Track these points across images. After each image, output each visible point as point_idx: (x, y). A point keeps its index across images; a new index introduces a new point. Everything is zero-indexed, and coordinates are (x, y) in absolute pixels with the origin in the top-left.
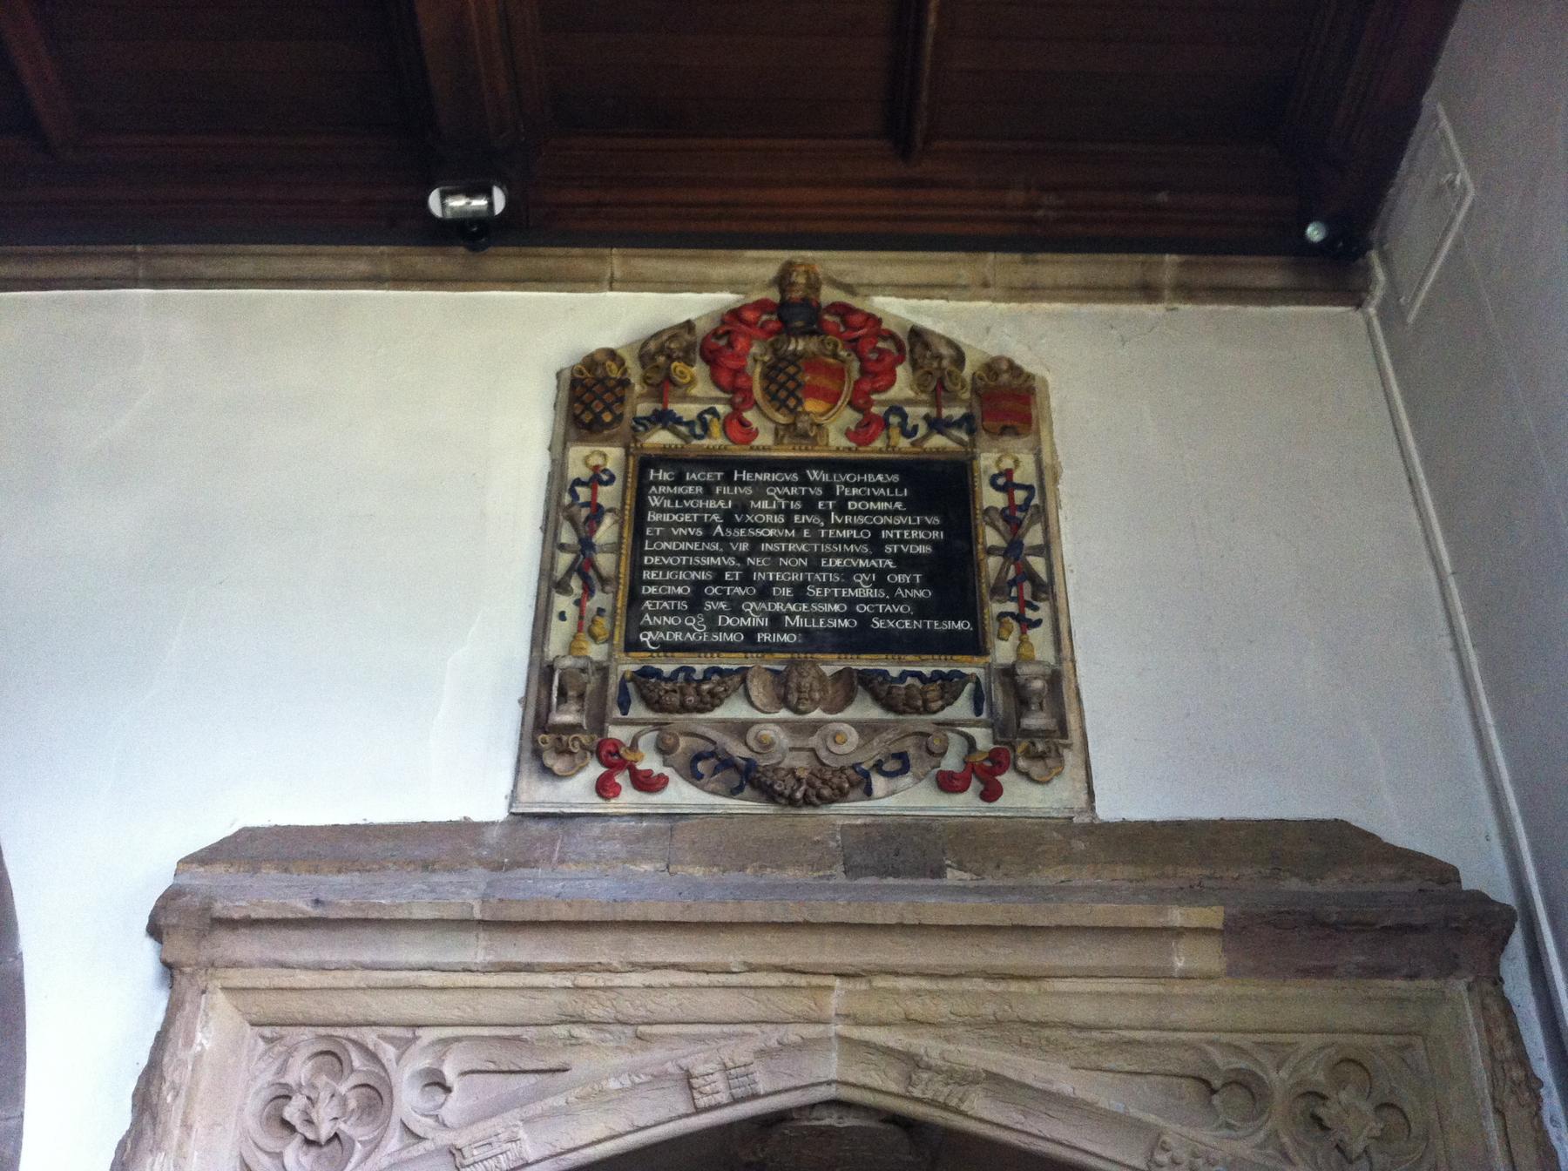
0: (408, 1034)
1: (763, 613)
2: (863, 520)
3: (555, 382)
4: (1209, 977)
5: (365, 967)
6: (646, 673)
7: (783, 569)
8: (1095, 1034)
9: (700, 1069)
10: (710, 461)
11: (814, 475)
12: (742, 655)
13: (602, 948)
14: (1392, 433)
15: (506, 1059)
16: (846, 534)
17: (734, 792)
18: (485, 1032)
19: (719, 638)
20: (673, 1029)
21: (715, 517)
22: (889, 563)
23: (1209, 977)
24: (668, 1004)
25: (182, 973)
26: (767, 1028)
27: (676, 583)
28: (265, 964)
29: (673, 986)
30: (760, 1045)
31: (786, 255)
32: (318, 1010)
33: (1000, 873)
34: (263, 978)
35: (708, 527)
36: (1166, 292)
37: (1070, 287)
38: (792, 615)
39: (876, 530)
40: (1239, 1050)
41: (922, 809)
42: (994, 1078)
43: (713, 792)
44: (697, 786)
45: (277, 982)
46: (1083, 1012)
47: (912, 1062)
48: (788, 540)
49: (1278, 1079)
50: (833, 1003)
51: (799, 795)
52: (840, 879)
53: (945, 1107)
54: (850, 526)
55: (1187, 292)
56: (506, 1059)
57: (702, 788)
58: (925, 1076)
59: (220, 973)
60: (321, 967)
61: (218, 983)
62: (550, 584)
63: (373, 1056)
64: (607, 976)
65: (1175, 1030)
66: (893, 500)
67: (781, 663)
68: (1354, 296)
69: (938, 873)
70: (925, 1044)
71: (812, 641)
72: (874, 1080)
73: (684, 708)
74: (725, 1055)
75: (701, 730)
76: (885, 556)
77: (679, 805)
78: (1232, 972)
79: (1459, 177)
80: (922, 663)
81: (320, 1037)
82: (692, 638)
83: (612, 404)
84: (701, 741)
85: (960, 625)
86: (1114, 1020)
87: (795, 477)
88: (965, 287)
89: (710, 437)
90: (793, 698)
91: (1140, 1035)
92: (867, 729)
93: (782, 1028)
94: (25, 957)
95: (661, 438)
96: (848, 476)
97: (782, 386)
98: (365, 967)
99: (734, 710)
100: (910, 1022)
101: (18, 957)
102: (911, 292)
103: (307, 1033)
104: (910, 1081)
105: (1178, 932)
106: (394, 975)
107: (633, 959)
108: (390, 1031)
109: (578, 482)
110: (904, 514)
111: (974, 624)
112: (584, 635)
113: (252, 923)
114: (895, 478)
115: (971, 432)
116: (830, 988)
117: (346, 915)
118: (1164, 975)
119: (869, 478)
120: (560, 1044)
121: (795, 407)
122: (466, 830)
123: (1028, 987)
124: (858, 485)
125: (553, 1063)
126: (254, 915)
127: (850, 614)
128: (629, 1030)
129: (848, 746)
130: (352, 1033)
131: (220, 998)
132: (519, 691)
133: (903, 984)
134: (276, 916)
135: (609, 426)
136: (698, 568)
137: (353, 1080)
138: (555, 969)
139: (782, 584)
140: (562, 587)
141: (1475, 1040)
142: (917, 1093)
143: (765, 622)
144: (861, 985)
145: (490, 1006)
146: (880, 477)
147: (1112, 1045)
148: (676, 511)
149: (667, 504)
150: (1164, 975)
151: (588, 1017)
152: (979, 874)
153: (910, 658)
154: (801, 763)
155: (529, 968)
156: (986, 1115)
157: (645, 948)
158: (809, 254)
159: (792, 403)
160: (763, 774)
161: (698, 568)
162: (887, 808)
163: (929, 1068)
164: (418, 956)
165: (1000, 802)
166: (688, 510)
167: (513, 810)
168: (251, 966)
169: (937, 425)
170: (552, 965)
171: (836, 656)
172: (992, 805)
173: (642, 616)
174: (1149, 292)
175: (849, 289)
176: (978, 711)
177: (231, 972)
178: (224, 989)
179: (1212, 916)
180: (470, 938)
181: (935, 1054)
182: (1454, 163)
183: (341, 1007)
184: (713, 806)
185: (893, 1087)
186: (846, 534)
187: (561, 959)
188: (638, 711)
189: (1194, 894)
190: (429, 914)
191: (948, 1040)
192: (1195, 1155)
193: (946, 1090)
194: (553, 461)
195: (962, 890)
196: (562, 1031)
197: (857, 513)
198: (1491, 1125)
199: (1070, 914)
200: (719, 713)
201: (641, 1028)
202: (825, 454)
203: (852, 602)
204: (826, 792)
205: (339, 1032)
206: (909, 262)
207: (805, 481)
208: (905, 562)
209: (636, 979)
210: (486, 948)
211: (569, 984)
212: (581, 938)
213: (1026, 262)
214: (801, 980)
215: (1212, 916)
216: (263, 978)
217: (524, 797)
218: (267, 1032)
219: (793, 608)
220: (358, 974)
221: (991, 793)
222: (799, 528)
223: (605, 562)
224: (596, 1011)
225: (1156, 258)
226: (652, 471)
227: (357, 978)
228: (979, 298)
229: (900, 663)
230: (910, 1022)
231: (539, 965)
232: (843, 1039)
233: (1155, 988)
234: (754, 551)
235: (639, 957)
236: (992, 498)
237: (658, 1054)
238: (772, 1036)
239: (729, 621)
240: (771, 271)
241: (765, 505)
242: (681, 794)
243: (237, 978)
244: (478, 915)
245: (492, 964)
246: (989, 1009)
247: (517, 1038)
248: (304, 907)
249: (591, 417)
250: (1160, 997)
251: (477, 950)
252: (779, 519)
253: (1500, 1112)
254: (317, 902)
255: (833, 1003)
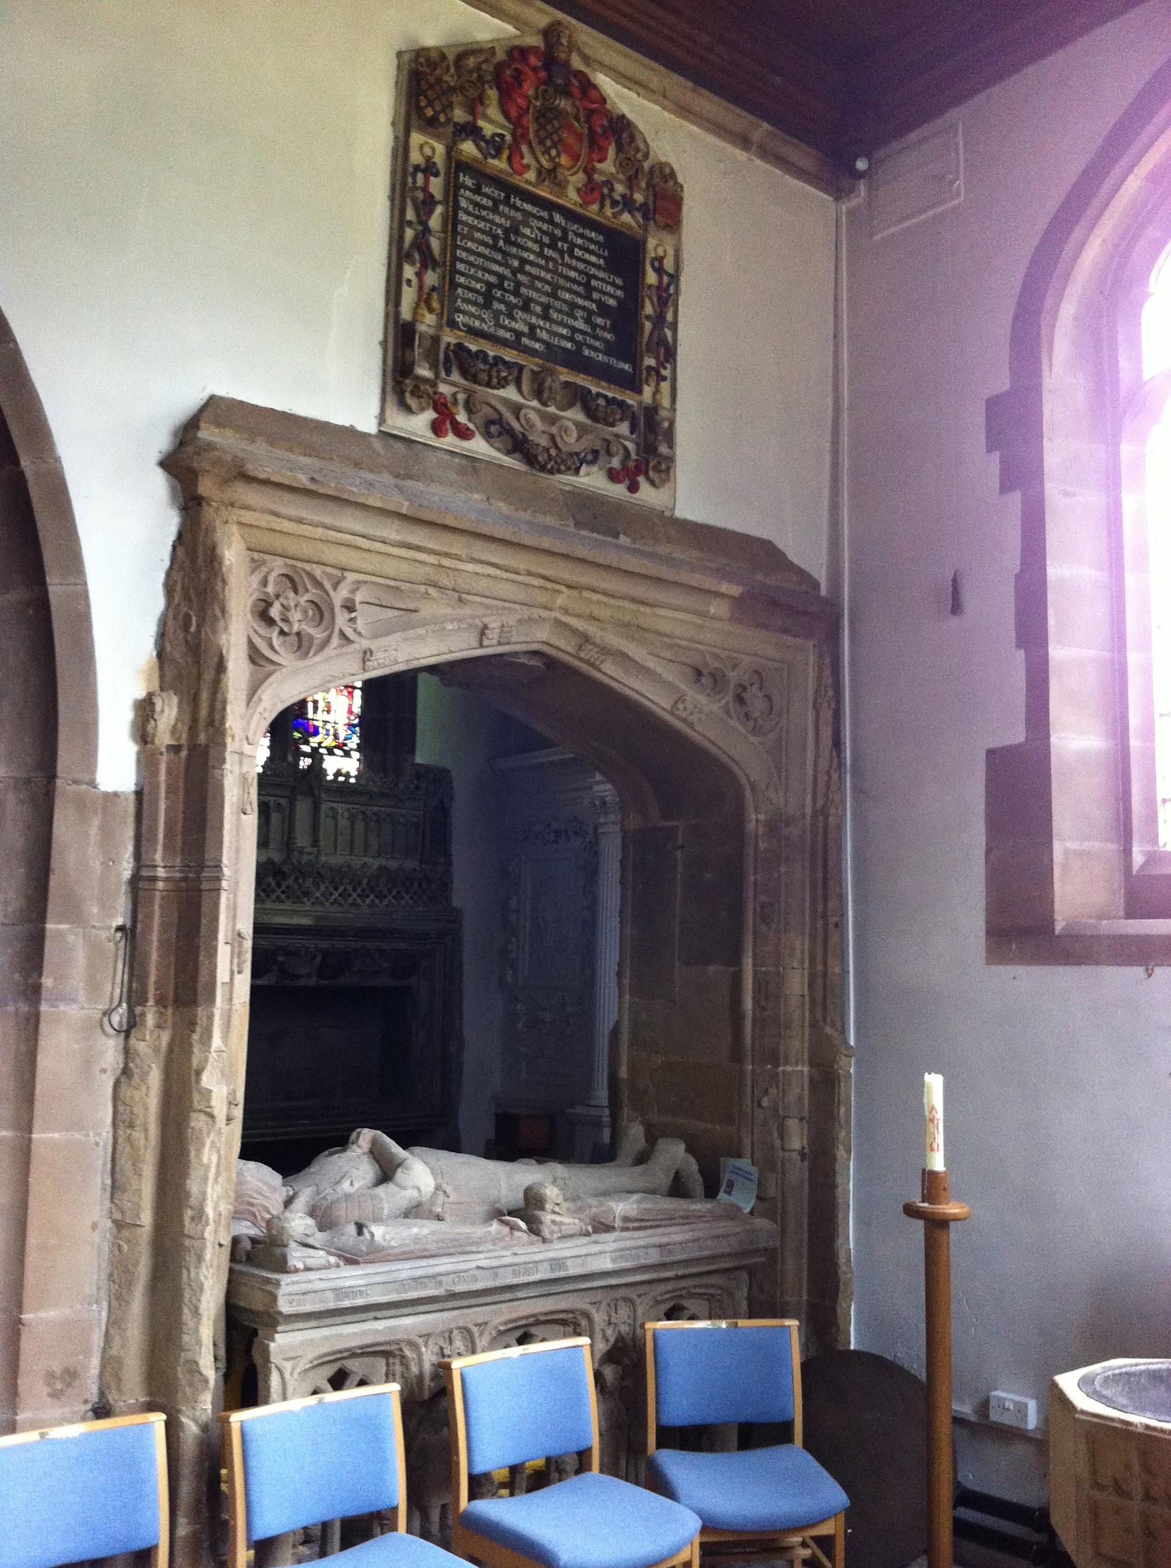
0: (338, 573)
1: (524, 321)
2: (581, 266)
3: (395, 61)
4: (721, 619)
5: (325, 527)
6: (460, 346)
7: (537, 290)
8: (666, 639)
9: (492, 625)
10: (498, 182)
11: (558, 218)
12: (516, 353)
13: (457, 545)
14: (832, 299)
15: (387, 599)
16: (572, 274)
17: (508, 453)
18: (382, 581)
19: (502, 333)
20: (478, 599)
21: (499, 231)
22: (594, 306)
23: (721, 619)
24: (482, 585)
25: (210, 505)
26: (525, 608)
27: (478, 280)
28: (264, 511)
29: (489, 576)
30: (518, 616)
31: (560, 15)
32: (290, 545)
33: (642, 542)
34: (264, 520)
35: (495, 238)
36: (754, 147)
37: (708, 120)
38: (541, 328)
39: (590, 277)
40: (717, 656)
41: (599, 489)
42: (623, 655)
43: (498, 450)
44: (488, 442)
45: (273, 525)
46: (664, 627)
47: (586, 638)
48: (541, 267)
49: (733, 675)
50: (560, 601)
51: (549, 466)
52: (572, 529)
53: (592, 665)
54: (575, 269)
55: (766, 153)
56: (387, 599)
57: (491, 445)
58: (590, 647)
59: (236, 511)
60: (300, 521)
61: (235, 518)
62: (398, 255)
63: (319, 585)
64: (456, 562)
65: (699, 643)
66: (599, 256)
67: (536, 365)
68: (839, 193)
69: (617, 536)
70: (592, 629)
71: (552, 354)
72: (562, 644)
73: (489, 384)
74: (504, 618)
75: (494, 402)
76: (592, 300)
77: (477, 453)
78: (732, 620)
79: (958, 182)
80: (609, 389)
81: (287, 565)
82: (486, 328)
83: (434, 100)
84: (492, 410)
85: (626, 367)
86: (677, 633)
87: (545, 214)
88: (653, 91)
89: (500, 160)
90: (546, 395)
91: (683, 643)
92: (582, 429)
93: (532, 609)
94: (63, 460)
95: (468, 148)
96: (576, 226)
97: (549, 136)
98: (325, 527)
99: (510, 393)
100: (592, 618)
101: (58, 460)
102: (621, 80)
103: (279, 562)
104: (580, 648)
105: (717, 594)
106: (340, 535)
107: (473, 556)
108: (328, 569)
109: (417, 168)
110: (604, 270)
111: (634, 370)
112: (423, 304)
113: (266, 482)
114: (601, 238)
115: (646, 217)
116: (562, 592)
117: (330, 493)
118: (705, 615)
119: (587, 232)
120: (418, 596)
121: (555, 157)
122: (350, 433)
123: (648, 610)
124: (582, 236)
125: (411, 606)
126: (273, 479)
127: (571, 339)
128: (456, 595)
129: (571, 441)
130: (307, 567)
131: (234, 529)
132: (379, 336)
133: (595, 597)
134: (287, 482)
135: (442, 125)
136: (490, 272)
137: (307, 597)
138: (431, 552)
139: (537, 303)
140: (409, 257)
141: (811, 673)
142: (582, 655)
143: (526, 329)
144: (575, 593)
145: (391, 568)
146: (593, 235)
147: (671, 646)
148: (477, 217)
149: (471, 208)
150: (705, 615)
151: (440, 584)
152: (634, 540)
153: (603, 384)
154: (544, 441)
155: (418, 549)
156: (610, 672)
157: (481, 550)
158: (574, 22)
159: (553, 152)
160: (532, 448)
161: (490, 272)
162: (583, 484)
163: (594, 644)
164: (358, 527)
165: (637, 495)
166: (483, 219)
167: (382, 429)
168: (255, 510)
169: (627, 204)
170: (430, 549)
171: (566, 370)
172: (633, 495)
173: (456, 301)
174: (744, 142)
175: (587, 60)
176: (632, 432)
177: (243, 512)
178: (240, 523)
179: (735, 590)
180: (388, 521)
181: (598, 635)
182: (957, 171)
183: (306, 550)
184: (495, 458)
185: (569, 649)
186: (572, 274)
187: (437, 547)
188: (456, 376)
189: (722, 573)
190: (378, 504)
191: (602, 629)
192: (695, 707)
193: (596, 656)
194: (396, 138)
195: (628, 549)
196: (423, 588)
197: (579, 259)
198: (811, 715)
199: (684, 577)
200: (501, 393)
201: (464, 596)
202: (566, 204)
203: (574, 330)
204: (563, 468)
205: (299, 564)
206: (626, 56)
207: (551, 221)
208: (603, 309)
209: (470, 567)
210: (396, 531)
211: (436, 563)
212: (449, 537)
213: (693, 90)
214: (549, 585)
215: (735, 590)
216: (264, 520)
217: (389, 422)
218: (256, 555)
219: (542, 323)
220: (320, 530)
221: (633, 488)
222: (547, 259)
223: (435, 244)
224: (445, 582)
225: (759, 122)
226: (461, 174)
227: (320, 532)
228: (656, 102)
229: (598, 386)
230: (592, 618)
231: (425, 548)
232: (557, 622)
233: (699, 621)
234: (521, 270)
235: (476, 555)
236: (651, 278)
237: (467, 611)
238: (526, 612)
239: (507, 322)
240: (543, 21)
241: (527, 231)
242: (479, 446)
243: (247, 517)
244: (404, 511)
245: (399, 542)
246: (627, 618)
247: (398, 588)
248: (303, 480)
249: (432, 113)
250: (702, 627)
251: (393, 531)
252: (536, 247)
253: (817, 709)
254: (313, 479)
255: (560, 601)
